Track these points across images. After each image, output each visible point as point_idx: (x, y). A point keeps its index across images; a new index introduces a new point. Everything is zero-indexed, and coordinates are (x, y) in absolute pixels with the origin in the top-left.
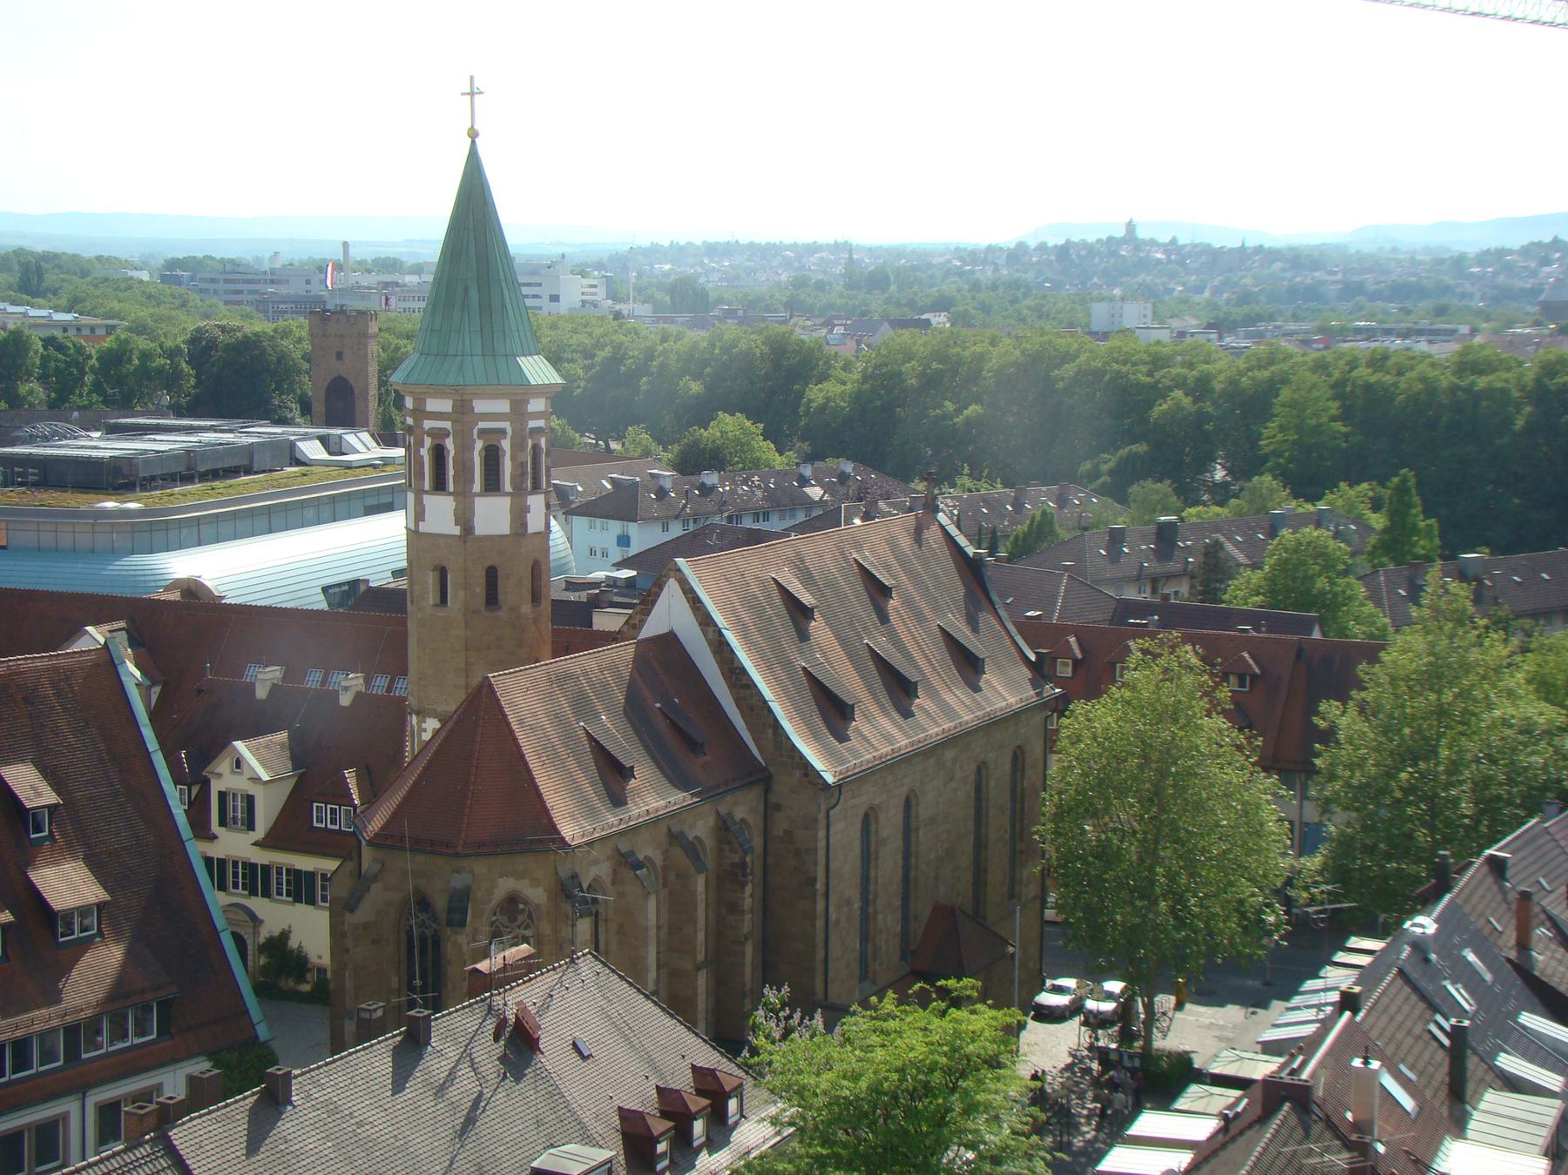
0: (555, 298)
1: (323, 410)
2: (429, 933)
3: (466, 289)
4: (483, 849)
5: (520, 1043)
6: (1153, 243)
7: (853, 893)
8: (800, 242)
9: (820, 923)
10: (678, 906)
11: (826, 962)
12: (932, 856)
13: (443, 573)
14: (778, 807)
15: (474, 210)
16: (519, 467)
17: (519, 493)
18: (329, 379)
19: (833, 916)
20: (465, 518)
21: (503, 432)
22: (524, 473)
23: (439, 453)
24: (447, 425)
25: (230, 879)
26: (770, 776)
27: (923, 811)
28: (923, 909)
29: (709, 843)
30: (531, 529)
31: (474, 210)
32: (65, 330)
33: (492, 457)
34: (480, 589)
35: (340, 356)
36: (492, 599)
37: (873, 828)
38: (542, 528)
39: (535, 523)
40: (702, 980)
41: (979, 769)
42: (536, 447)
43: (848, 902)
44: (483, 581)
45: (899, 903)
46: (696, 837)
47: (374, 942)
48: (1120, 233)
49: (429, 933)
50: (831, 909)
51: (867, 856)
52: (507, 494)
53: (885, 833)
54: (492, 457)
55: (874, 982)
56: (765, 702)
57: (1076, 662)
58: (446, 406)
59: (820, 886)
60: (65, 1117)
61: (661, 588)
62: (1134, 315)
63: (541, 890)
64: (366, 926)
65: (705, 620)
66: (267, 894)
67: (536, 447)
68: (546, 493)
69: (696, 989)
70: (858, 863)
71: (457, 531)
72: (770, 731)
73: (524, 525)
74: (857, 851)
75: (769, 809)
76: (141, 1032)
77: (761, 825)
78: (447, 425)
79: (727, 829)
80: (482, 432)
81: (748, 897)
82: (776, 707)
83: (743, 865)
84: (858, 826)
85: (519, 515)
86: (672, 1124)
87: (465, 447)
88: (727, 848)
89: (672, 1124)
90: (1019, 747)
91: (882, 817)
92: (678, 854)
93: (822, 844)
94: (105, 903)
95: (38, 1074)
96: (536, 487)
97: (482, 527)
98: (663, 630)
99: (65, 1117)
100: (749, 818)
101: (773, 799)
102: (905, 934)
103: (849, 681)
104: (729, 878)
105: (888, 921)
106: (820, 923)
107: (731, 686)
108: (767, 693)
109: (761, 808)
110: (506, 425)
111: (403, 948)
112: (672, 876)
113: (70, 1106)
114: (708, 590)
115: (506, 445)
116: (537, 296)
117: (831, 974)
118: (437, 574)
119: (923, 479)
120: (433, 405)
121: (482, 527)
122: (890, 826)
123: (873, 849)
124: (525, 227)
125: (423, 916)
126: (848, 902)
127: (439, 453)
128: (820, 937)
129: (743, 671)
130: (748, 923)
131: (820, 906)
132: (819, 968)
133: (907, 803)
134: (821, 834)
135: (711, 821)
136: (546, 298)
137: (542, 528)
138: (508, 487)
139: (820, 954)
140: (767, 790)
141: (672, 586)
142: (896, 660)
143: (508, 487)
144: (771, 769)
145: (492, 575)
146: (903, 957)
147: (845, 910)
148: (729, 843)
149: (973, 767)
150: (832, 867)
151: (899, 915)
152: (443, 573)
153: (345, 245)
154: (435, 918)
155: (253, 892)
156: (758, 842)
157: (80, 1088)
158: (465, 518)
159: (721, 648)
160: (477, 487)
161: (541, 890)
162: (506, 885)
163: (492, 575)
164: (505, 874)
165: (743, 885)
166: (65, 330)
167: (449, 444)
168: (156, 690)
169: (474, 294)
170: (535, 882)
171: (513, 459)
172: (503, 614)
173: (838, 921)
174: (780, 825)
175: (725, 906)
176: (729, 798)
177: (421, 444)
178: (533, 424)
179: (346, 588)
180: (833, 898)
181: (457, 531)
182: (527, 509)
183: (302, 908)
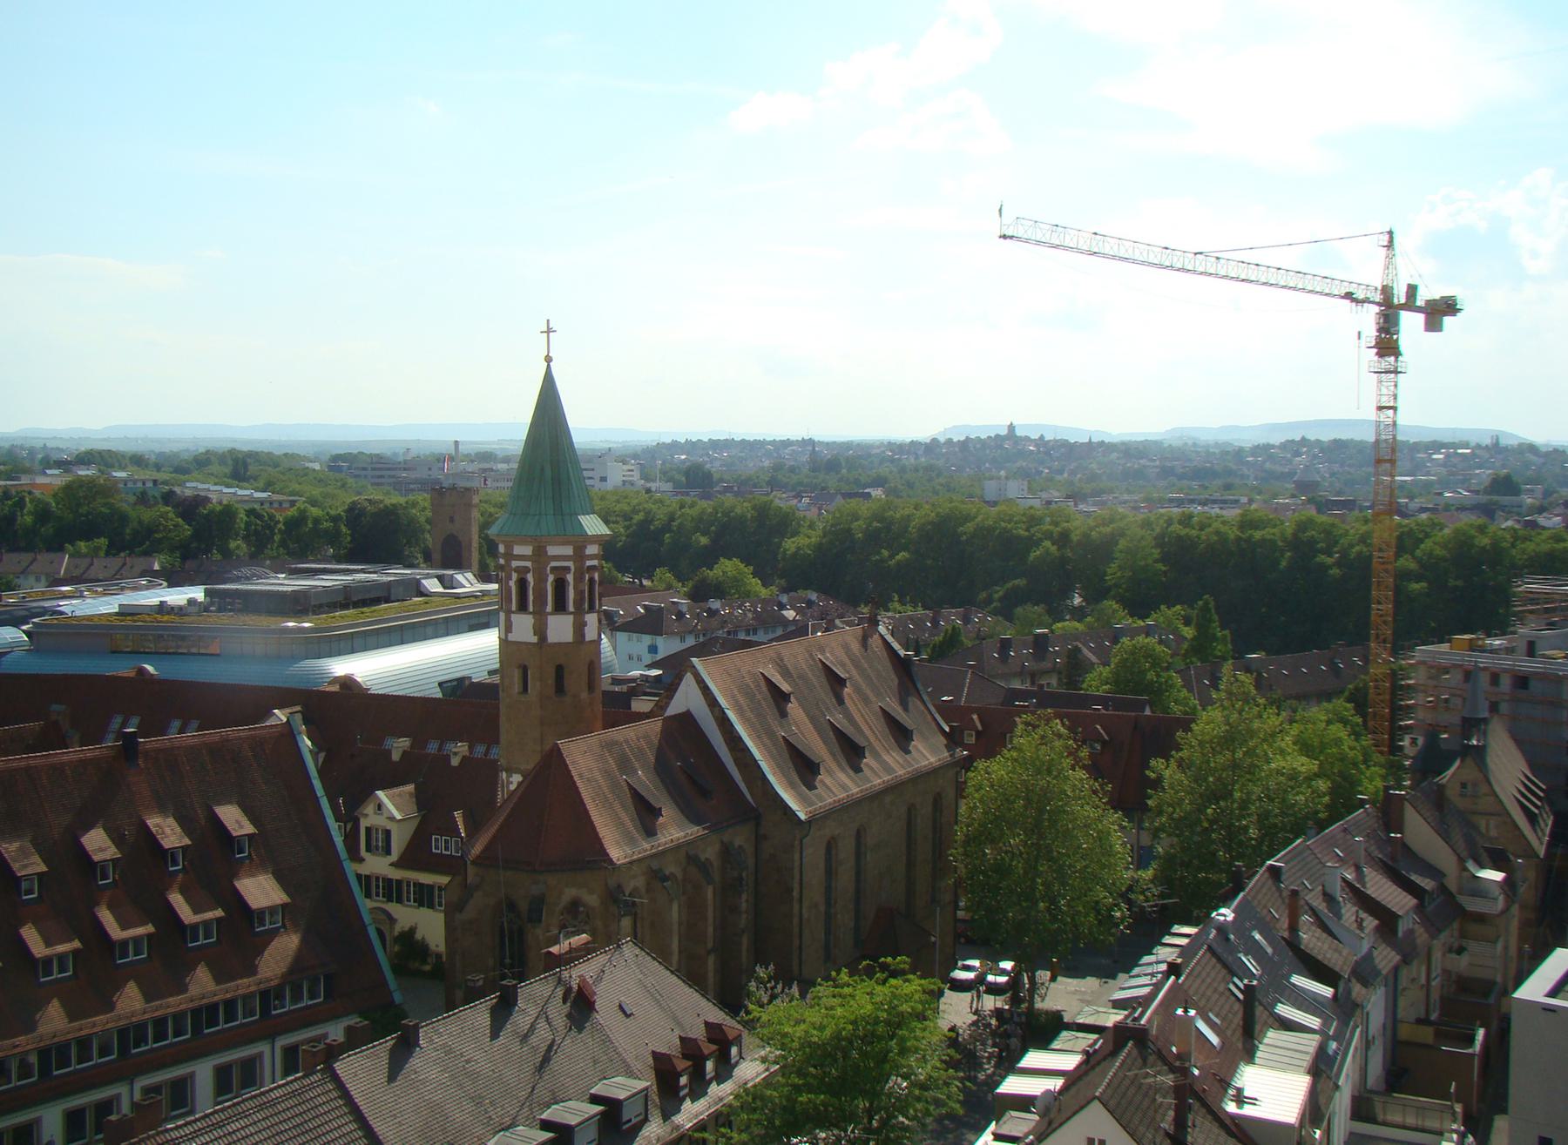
0: (604, 479)
5: (581, 1005)
9: (796, 921)
11: (800, 948)
13: (525, 670)
15: (549, 406)
17: (579, 612)
19: (805, 916)
20: (540, 630)
21: (567, 569)
22: (582, 599)
23: (522, 584)
24: (528, 564)
31: (549, 406)
33: (560, 586)
34: (551, 681)
35: (452, 520)
36: (560, 688)
39: (590, 633)
40: (711, 961)
54: (560, 586)
59: (795, 894)
60: (261, 1055)
65: (712, 702)
66: (399, 900)
71: (535, 639)
75: (759, 839)
76: (177, 1033)
78: (528, 564)
80: (554, 569)
81: (744, 901)
83: (741, 879)
85: (579, 628)
87: (541, 580)
93: (797, 864)
99: (261, 1055)
103: (816, 746)
110: (570, 564)
113: (263, 1048)
115: (570, 578)
127: (522, 584)
128: (796, 930)
133: (858, 832)
135: (717, 847)
138: (571, 609)
139: (796, 942)
140: (758, 825)
141: (689, 678)
143: (571, 609)
145: (560, 670)
152: (525, 670)
155: (390, 900)
156: (751, 862)
157: (271, 1036)
158: (540, 630)
160: (549, 608)
162: (570, 893)
163: (560, 670)
167: (530, 577)
178: (589, 563)
181: (535, 639)
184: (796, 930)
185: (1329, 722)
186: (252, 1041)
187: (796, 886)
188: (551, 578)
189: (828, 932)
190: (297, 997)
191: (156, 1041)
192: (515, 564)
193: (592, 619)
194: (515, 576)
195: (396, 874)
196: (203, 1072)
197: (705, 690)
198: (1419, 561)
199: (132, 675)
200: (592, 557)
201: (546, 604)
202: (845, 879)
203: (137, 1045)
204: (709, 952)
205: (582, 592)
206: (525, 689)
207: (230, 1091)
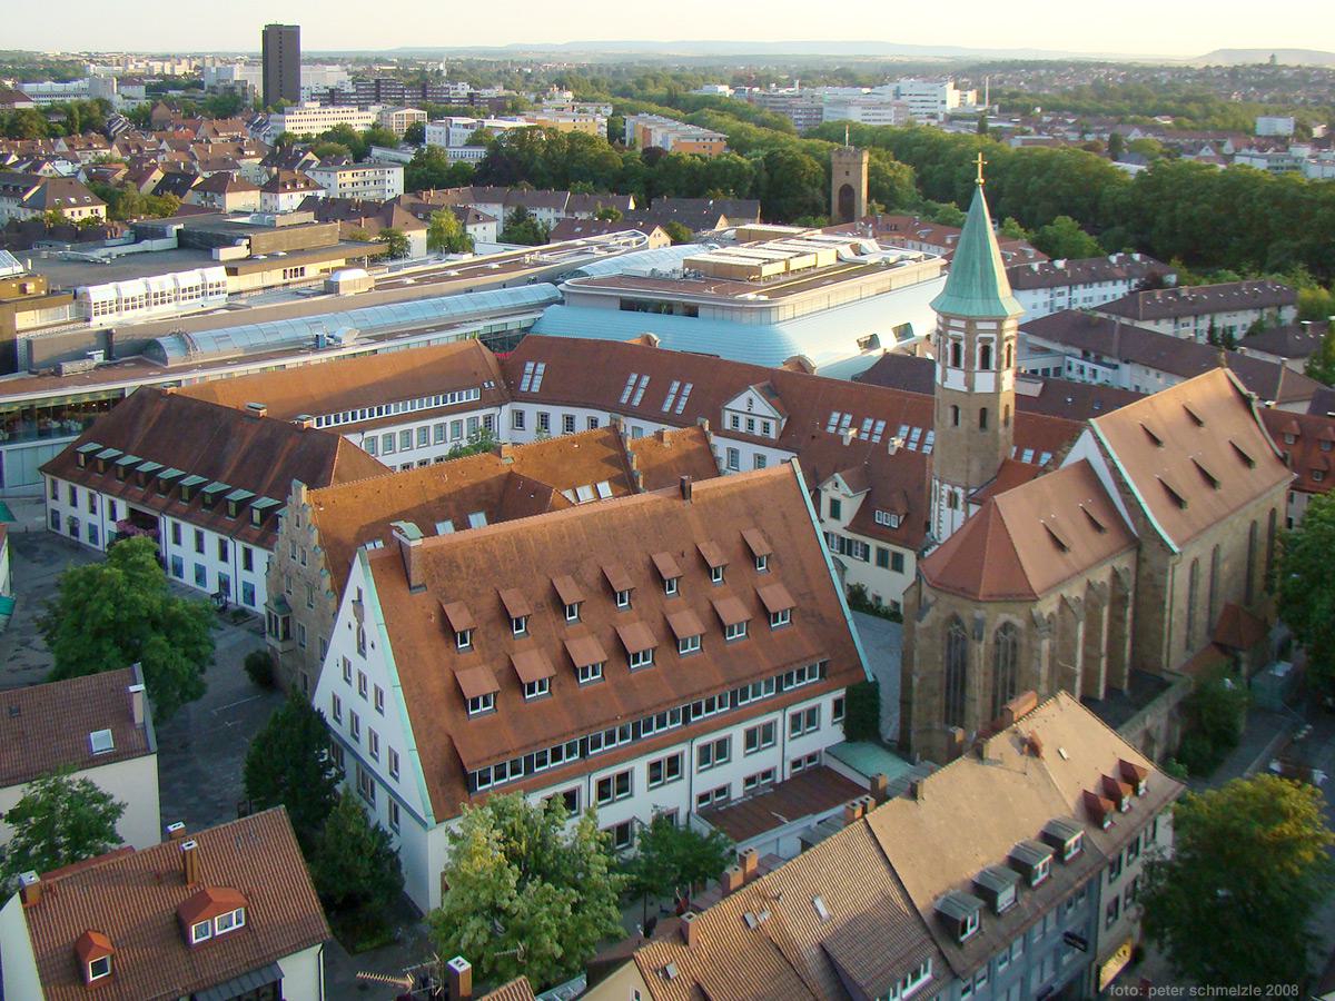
0: (944, 102)
3: (974, 265)
4: (992, 598)
5: (1033, 749)
6: (1284, 67)
9: (1166, 625)
11: (1169, 647)
13: (956, 409)
14: (1145, 560)
19: (1173, 619)
20: (969, 383)
21: (992, 340)
23: (956, 348)
24: (962, 334)
27: (1222, 554)
28: (1220, 608)
32: (698, 140)
34: (977, 420)
35: (847, 173)
36: (983, 424)
42: (1009, 346)
48: (1266, 61)
51: (1193, 583)
53: (1201, 571)
54: (986, 352)
56: (1139, 503)
57: (1297, 437)
58: (962, 324)
59: (1167, 606)
64: (927, 629)
65: (1106, 455)
66: (849, 554)
67: (1009, 346)
69: (1099, 666)
71: (965, 389)
78: (962, 334)
80: (981, 340)
82: (1145, 506)
87: (971, 346)
93: (1169, 583)
101: (1142, 555)
102: (1210, 623)
103: (1186, 484)
104: (1118, 602)
105: (1201, 617)
107: (1120, 492)
108: (1141, 499)
112: (1089, 605)
113: (776, 716)
114: (1106, 436)
116: (935, 95)
118: (957, 973)
120: (954, 323)
122: (1205, 567)
125: (957, 627)
126: (1181, 611)
127: (956, 348)
128: (1166, 633)
129: (1127, 485)
131: (1167, 616)
132: (1165, 649)
133: (1214, 550)
134: (1169, 578)
138: (994, 369)
139: (1166, 641)
141: (1087, 434)
144: (1143, 540)
145: (984, 412)
150: (1175, 593)
152: (956, 409)
154: (963, 628)
155: (842, 552)
158: (969, 383)
159: (1114, 470)
160: (977, 367)
162: (1003, 618)
163: (984, 412)
165: (1126, 608)
166: (698, 140)
167: (963, 344)
168: (785, 420)
169: (978, 265)
172: (988, 434)
174: (1145, 570)
175: (1117, 619)
177: (946, 342)
180: (1174, 610)
181: (965, 389)
184: (1166, 633)
186: (770, 711)
187: (1168, 601)
188: (979, 346)
192: (951, 333)
194: (951, 341)
195: (848, 535)
196: (737, 734)
197: (1097, 438)
199: (636, 341)
201: (974, 364)
206: (956, 422)
207: (755, 746)
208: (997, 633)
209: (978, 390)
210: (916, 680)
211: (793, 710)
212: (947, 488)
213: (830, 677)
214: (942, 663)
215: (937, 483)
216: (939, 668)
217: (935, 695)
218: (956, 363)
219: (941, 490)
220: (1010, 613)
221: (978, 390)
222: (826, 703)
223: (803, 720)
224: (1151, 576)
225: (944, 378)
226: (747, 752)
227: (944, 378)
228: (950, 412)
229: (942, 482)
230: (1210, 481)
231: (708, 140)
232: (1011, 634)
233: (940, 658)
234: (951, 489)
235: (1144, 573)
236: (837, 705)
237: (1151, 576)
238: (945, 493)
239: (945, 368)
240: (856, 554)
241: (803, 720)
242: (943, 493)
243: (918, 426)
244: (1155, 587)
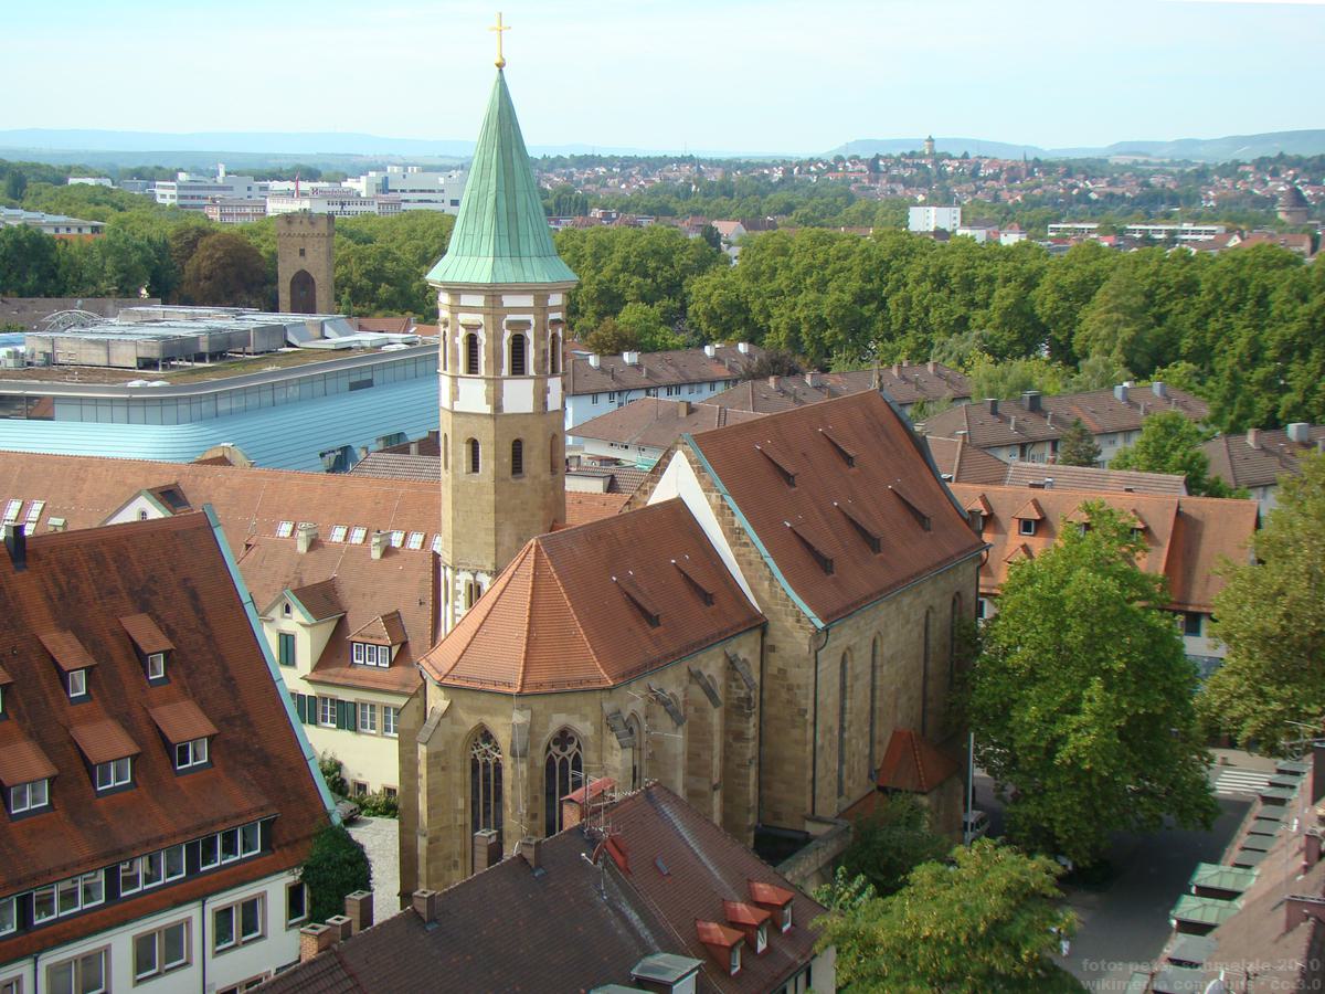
1: (289, 299)
2: (491, 762)
7: (834, 722)
8: (652, 155)
10: (698, 736)
11: (814, 780)
12: (893, 688)
13: (474, 444)
14: (773, 649)
15: (505, 122)
16: (541, 353)
17: (541, 377)
18: (298, 269)
19: (819, 742)
21: (528, 323)
22: (545, 359)
23: (472, 342)
25: (320, 714)
26: (766, 622)
28: (884, 732)
29: (720, 681)
30: (551, 408)
31: (505, 122)
33: (518, 345)
34: (507, 460)
35: (302, 253)
37: (849, 665)
38: (559, 407)
39: (554, 402)
40: (717, 799)
41: (928, 613)
43: (830, 730)
44: (510, 452)
45: (867, 729)
46: (709, 676)
47: (443, 769)
49: (491, 762)
50: (818, 735)
52: (531, 378)
54: (518, 345)
55: (848, 797)
58: (479, 301)
60: (188, 921)
61: (669, 459)
62: (214, 214)
63: (588, 724)
68: (564, 375)
69: (712, 808)
70: (838, 695)
72: (766, 583)
73: (545, 404)
74: (838, 686)
75: (766, 650)
76: (246, 848)
77: (759, 663)
79: (735, 669)
80: (511, 324)
81: (751, 729)
83: (749, 699)
84: (839, 665)
85: (541, 395)
86: (742, 934)
88: (734, 684)
89: (742, 934)
90: (958, 593)
91: (856, 655)
92: (696, 691)
94: (215, 735)
95: (166, 885)
96: (554, 371)
97: (509, 407)
98: (671, 496)
99: (188, 921)
100: (750, 659)
101: (769, 641)
102: (10, 554)
105: (858, 744)
106: (810, 748)
109: (759, 649)
110: (530, 317)
111: (469, 774)
113: (192, 911)
115: (530, 334)
117: (817, 791)
118: (470, 446)
119: (1127, 381)
121: (509, 407)
123: (848, 684)
124: (540, 140)
125: (486, 746)
126: (830, 730)
127: (472, 342)
130: (751, 749)
135: (721, 661)
136: (448, 202)
137: (559, 407)
138: (532, 372)
140: (764, 634)
142: (861, 518)
143: (532, 372)
145: (517, 447)
146: (870, 776)
147: (828, 736)
148: (736, 680)
149: (924, 611)
151: (867, 738)
152: (474, 444)
153: (931, 140)
156: (756, 678)
157: (202, 897)
160: (506, 371)
161: (588, 724)
163: (517, 447)
164: (558, 710)
167: (482, 335)
170: (584, 718)
171: (536, 346)
172: (526, 481)
173: (822, 747)
175: (734, 736)
176: (734, 641)
177: (455, 333)
178: (552, 316)
179: (339, 453)
181: (488, 409)
182: (546, 391)
183: (346, 734)
185: (1294, 556)
186: (178, 903)
188: (507, 334)
189: (841, 761)
190: (229, 849)
191: (147, 882)
193: (555, 384)
194: (463, 332)
198: (1252, 875)
200: (555, 309)
202: (859, 700)
203: (204, 864)
204: (715, 788)
205: (545, 351)
206: (475, 468)
208: (549, 748)
209: (508, 408)
210: (422, 843)
211: (218, 902)
212: (465, 577)
213: (279, 847)
214: (465, 811)
215: (449, 571)
216: (460, 820)
217: (455, 864)
218: (472, 367)
219: (455, 581)
220: (570, 711)
221: (508, 408)
222: (275, 891)
223: (237, 919)
224: (782, 671)
225: (455, 396)
226: (139, 977)
227: (455, 396)
228: (464, 451)
229: (456, 571)
230: (872, 542)
231: (74, 231)
232: (572, 748)
233: (461, 804)
234: (471, 578)
235: (772, 670)
236: (294, 894)
237: (782, 671)
238: (462, 588)
239: (454, 378)
240: (324, 720)
241: (237, 919)
242: (458, 587)
243: (417, 530)
244: (790, 688)
